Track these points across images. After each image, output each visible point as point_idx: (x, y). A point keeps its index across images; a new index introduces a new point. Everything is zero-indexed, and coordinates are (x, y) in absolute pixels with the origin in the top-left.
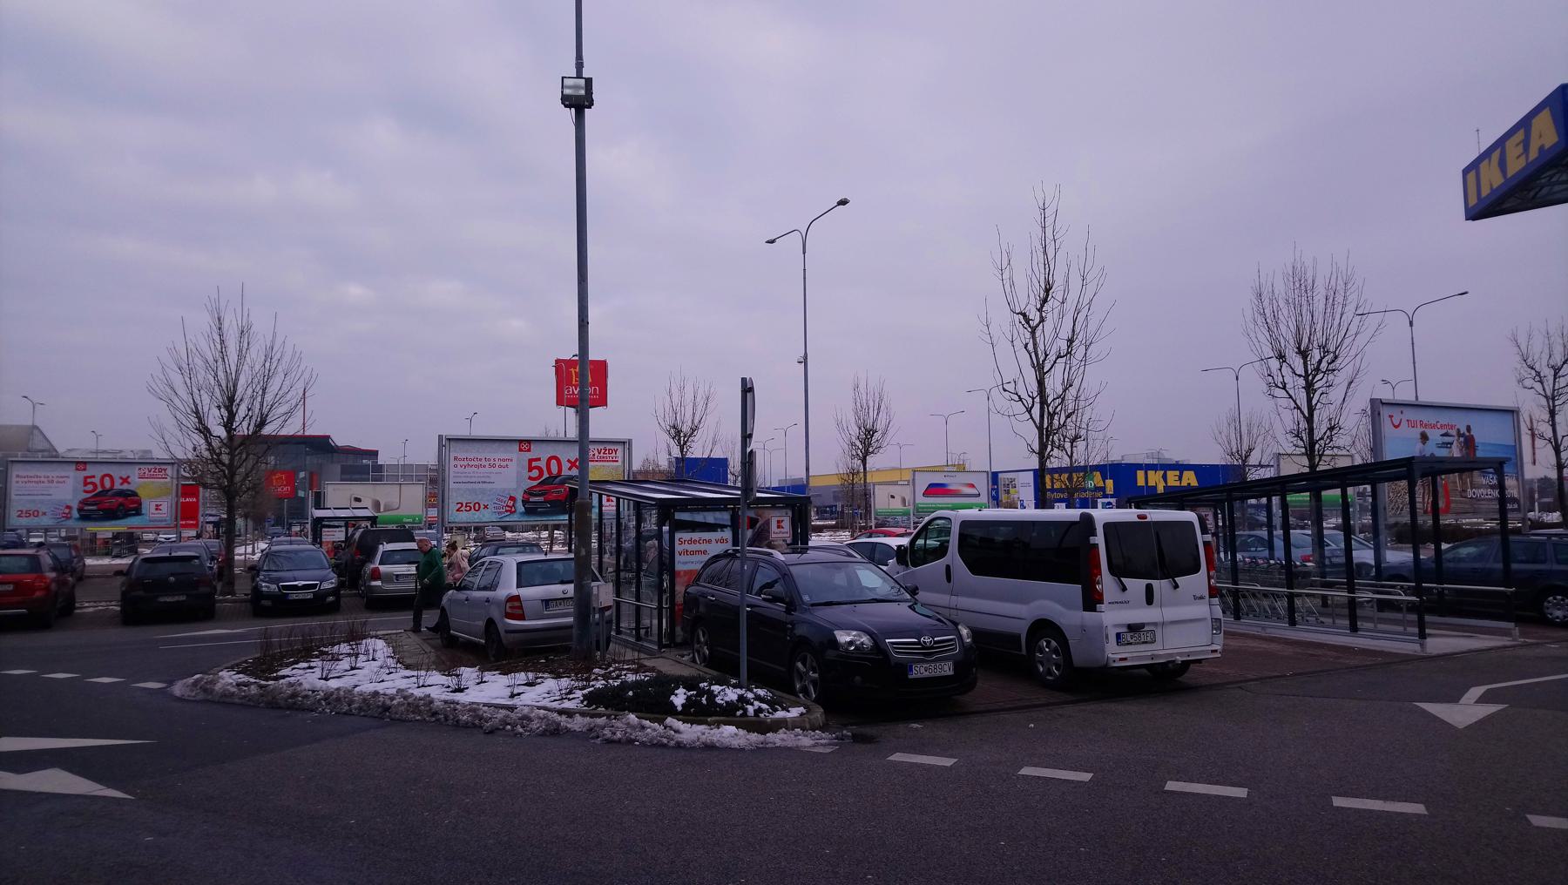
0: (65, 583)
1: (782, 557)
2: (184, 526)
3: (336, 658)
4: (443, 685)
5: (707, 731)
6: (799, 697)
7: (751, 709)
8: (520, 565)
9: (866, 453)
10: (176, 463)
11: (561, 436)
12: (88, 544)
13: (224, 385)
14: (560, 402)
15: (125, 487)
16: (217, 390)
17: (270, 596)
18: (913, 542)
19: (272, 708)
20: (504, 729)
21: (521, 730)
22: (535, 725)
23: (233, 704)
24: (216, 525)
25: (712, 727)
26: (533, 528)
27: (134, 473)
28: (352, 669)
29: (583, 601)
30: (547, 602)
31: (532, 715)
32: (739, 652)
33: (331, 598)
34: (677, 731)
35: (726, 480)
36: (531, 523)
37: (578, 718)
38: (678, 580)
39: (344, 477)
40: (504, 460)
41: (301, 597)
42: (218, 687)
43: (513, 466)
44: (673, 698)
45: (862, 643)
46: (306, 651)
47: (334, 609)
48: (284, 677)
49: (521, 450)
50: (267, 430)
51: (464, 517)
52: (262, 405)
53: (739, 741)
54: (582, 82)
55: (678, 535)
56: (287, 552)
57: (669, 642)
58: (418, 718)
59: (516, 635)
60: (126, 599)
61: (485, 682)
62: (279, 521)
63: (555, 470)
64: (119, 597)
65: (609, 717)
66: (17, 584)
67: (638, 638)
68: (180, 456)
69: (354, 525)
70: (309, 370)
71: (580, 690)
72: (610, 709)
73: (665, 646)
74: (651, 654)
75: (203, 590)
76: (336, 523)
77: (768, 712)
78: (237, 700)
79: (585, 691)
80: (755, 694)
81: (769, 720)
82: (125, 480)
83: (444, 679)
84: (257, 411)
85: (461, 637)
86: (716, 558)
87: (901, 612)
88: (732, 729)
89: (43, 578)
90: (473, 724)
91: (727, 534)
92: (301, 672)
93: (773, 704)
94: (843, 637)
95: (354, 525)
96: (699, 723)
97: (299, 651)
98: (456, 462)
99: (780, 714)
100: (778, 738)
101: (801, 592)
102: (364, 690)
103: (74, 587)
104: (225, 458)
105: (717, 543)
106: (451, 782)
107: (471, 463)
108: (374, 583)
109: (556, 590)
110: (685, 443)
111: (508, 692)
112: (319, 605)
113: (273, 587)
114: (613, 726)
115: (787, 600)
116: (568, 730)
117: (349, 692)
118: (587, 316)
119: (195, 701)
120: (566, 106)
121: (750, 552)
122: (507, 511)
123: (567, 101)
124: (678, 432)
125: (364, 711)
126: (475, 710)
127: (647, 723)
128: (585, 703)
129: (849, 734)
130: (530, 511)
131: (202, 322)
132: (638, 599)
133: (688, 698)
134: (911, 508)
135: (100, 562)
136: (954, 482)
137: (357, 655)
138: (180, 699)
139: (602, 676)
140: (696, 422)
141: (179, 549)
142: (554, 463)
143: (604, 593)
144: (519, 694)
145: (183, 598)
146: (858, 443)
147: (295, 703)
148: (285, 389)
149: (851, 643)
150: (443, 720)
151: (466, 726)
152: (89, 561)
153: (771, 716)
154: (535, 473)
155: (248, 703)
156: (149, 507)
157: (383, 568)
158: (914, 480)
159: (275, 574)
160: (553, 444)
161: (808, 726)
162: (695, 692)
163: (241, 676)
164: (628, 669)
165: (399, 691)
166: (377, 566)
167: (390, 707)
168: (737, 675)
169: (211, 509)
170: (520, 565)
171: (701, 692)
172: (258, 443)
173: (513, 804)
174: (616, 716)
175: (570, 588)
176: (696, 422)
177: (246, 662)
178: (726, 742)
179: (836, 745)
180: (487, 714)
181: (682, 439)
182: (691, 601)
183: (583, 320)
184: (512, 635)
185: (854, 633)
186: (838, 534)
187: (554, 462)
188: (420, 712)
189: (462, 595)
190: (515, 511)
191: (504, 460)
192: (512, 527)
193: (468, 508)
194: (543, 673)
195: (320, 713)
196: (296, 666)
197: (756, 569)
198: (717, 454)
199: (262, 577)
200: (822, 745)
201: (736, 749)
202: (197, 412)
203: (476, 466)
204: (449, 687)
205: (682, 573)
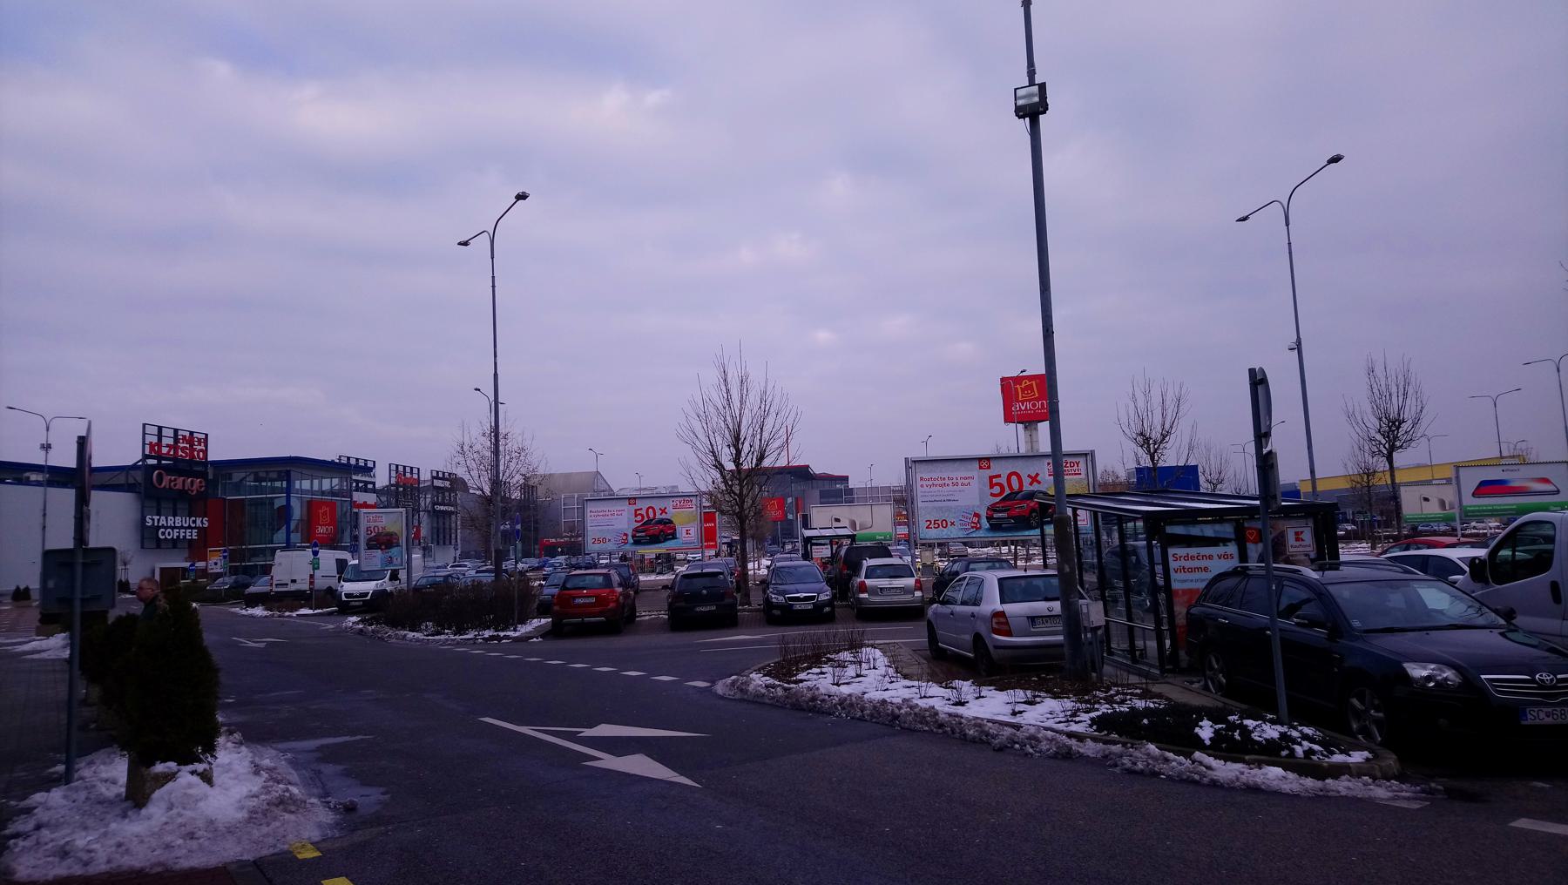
0: (629, 595)
1: (1314, 575)
2: (707, 547)
3: (842, 665)
4: (943, 697)
5: (1246, 771)
6: (1358, 739)
7: (1299, 750)
8: (1001, 581)
9: (1392, 449)
10: (699, 494)
11: (1014, 451)
12: (639, 563)
13: (731, 428)
14: (1008, 418)
15: (664, 516)
16: (727, 432)
17: (778, 606)
18: (1493, 554)
19: (797, 709)
20: (1012, 747)
21: (1031, 750)
22: (1044, 746)
23: (764, 703)
24: (729, 545)
25: (1252, 766)
26: (991, 544)
27: (669, 504)
28: (858, 676)
29: (1072, 618)
30: (1033, 619)
31: (1040, 736)
32: (1275, 686)
33: (827, 609)
34: (1209, 768)
35: (1197, 486)
36: (991, 539)
37: (1089, 743)
38: (1176, 600)
39: (822, 500)
40: (966, 478)
41: (803, 607)
42: (751, 688)
43: (974, 483)
44: (1197, 730)
45: (1446, 679)
46: (816, 659)
47: (829, 619)
48: (802, 681)
49: (981, 468)
50: (766, 463)
51: (934, 534)
52: (760, 440)
53: (1290, 786)
54: (1035, 89)
55: (1171, 551)
56: (789, 567)
57: (1169, 665)
58: (927, 728)
59: (1007, 651)
60: (672, 609)
61: (983, 697)
62: (775, 541)
63: (1016, 486)
64: (666, 608)
65: (1124, 745)
66: (597, 597)
67: (1135, 661)
68: (704, 489)
69: (837, 543)
70: (795, 408)
71: (1085, 712)
72: (1124, 737)
73: (1169, 671)
74: (1155, 679)
75: (728, 601)
76: (823, 542)
77: (1323, 755)
78: (767, 701)
79: (1093, 715)
80: (1301, 732)
81: (1325, 764)
82: (663, 511)
83: (947, 693)
84: (757, 447)
85: (950, 650)
86: (1222, 576)
87: (1490, 641)
88: (1278, 771)
89: (614, 592)
90: (980, 739)
91: (1232, 549)
92: (815, 677)
93: (1328, 746)
94: (1417, 671)
95: (837, 543)
96: (1235, 761)
97: (810, 657)
98: (922, 483)
99: (1338, 758)
100: (1342, 786)
101: (1348, 617)
102: (873, 698)
103: (634, 598)
104: (736, 489)
105: (1220, 560)
106: (973, 799)
107: (936, 482)
108: (862, 596)
109: (1040, 607)
110: (1156, 451)
111: (1008, 709)
112: (817, 615)
113: (781, 598)
114: (1131, 756)
115: (1329, 625)
116: (1081, 755)
117: (860, 698)
118: (1052, 326)
119: (735, 700)
120: (1019, 118)
121: (1276, 569)
122: (972, 527)
123: (1021, 112)
124: (1147, 440)
125: (875, 717)
126: (980, 726)
127: (1171, 755)
128: (1095, 727)
129: (1440, 787)
130: (995, 527)
131: (712, 376)
132: (1130, 619)
133: (1216, 732)
134: (1456, 512)
135: (649, 578)
136: (1516, 478)
137: (860, 663)
138: (722, 697)
139: (1104, 699)
140: (1167, 426)
141: (707, 566)
142: (1014, 479)
143: (1094, 612)
144: (1021, 712)
145: (714, 608)
146: (1379, 437)
147: (815, 706)
148: (777, 427)
149: (1429, 678)
150: (950, 732)
151: (973, 741)
152: (642, 578)
153: (1327, 760)
154: (997, 490)
155: (777, 704)
156: (681, 531)
157: (868, 582)
158: (1458, 478)
159: (781, 587)
160: (1011, 461)
161: (1379, 774)
162: (1224, 726)
163: (768, 678)
164: (1131, 694)
165: (905, 700)
166: (863, 579)
167: (899, 716)
168: (1274, 710)
169: (726, 534)
170: (1001, 581)
171: (1232, 727)
172: (759, 474)
173: (1041, 830)
174: (1132, 744)
175: (1056, 606)
176: (1167, 426)
177: (769, 665)
178: (1275, 784)
179: (1425, 799)
180: (993, 730)
181: (1152, 446)
182: (1196, 623)
183: (1047, 331)
184: (1002, 650)
185: (1433, 666)
186: (1351, 546)
187: (1014, 478)
188: (927, 723)
189: (947, 609)
190: (980, 528)
191: (966, 478)
192: (971, 542)
193: (937, 525)
194: (1039, 691)
195: (837, 717)
196: (810, 671)
197: (1281, 587)
198: (1192, 462)
199: (771, 590)
200: (1405, 798)
201: (1287, 794)
202: (713, 452)
203: (940, 485)
204: (949, 699)
205: (1180, 592)
